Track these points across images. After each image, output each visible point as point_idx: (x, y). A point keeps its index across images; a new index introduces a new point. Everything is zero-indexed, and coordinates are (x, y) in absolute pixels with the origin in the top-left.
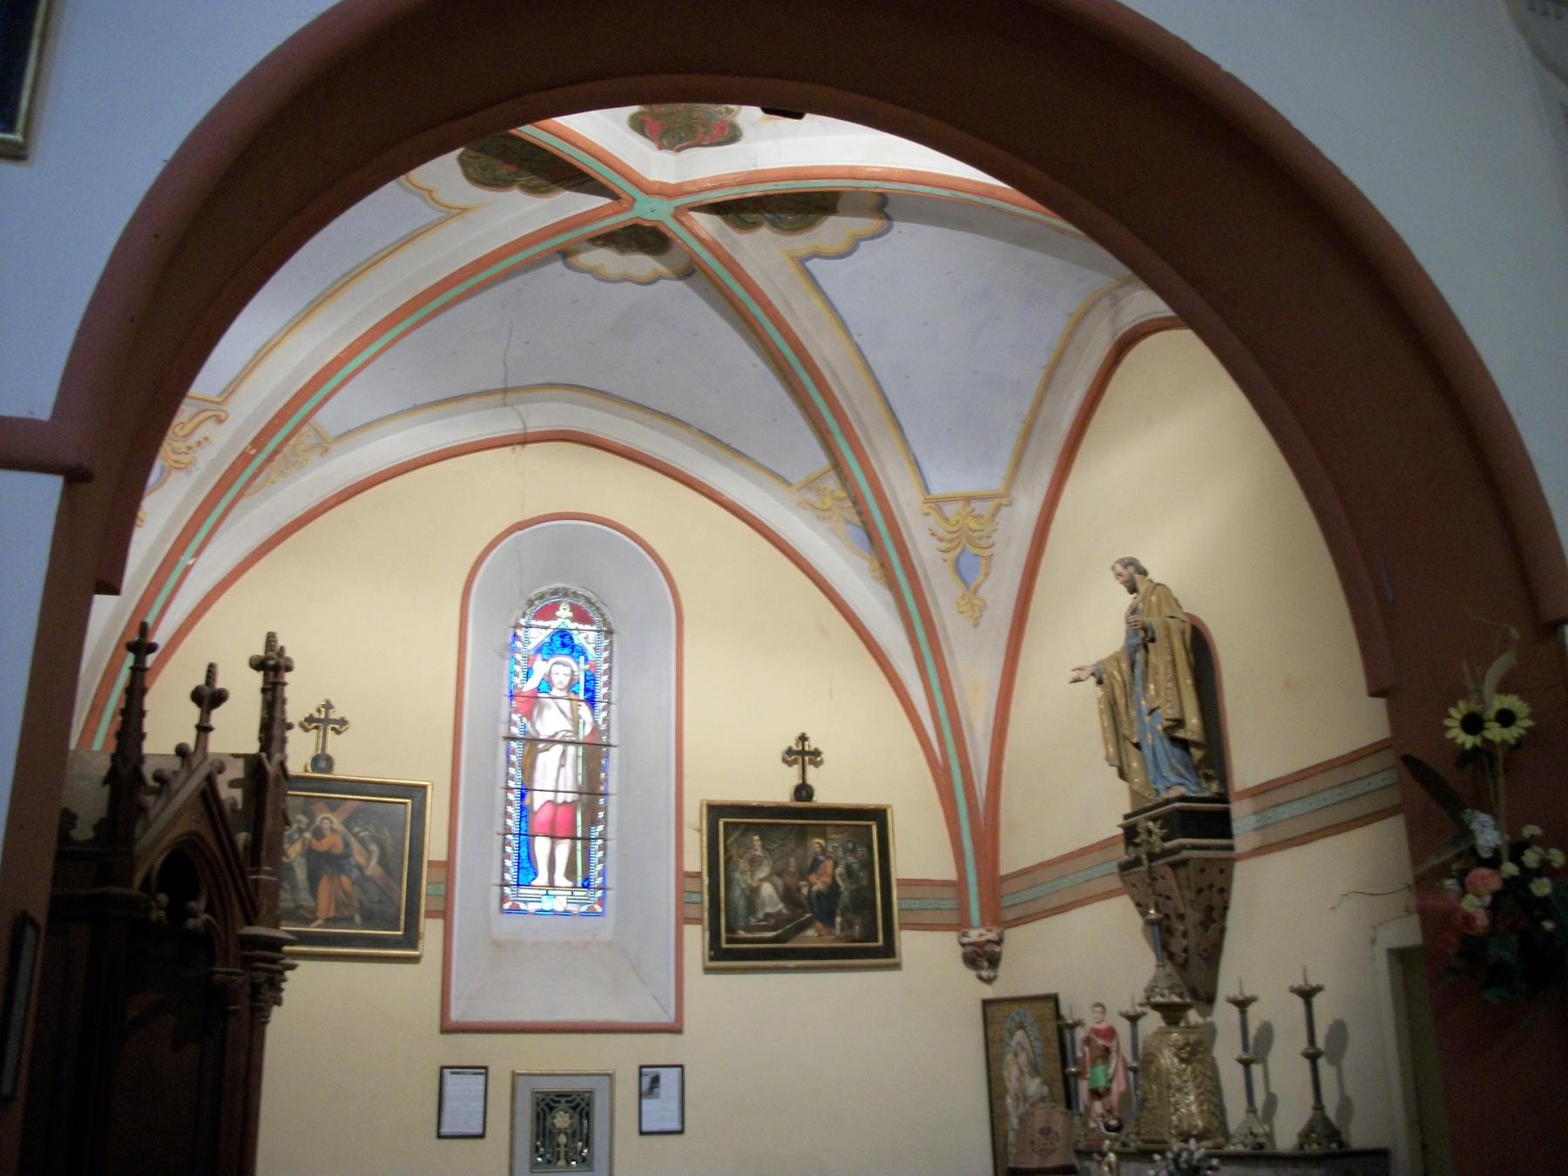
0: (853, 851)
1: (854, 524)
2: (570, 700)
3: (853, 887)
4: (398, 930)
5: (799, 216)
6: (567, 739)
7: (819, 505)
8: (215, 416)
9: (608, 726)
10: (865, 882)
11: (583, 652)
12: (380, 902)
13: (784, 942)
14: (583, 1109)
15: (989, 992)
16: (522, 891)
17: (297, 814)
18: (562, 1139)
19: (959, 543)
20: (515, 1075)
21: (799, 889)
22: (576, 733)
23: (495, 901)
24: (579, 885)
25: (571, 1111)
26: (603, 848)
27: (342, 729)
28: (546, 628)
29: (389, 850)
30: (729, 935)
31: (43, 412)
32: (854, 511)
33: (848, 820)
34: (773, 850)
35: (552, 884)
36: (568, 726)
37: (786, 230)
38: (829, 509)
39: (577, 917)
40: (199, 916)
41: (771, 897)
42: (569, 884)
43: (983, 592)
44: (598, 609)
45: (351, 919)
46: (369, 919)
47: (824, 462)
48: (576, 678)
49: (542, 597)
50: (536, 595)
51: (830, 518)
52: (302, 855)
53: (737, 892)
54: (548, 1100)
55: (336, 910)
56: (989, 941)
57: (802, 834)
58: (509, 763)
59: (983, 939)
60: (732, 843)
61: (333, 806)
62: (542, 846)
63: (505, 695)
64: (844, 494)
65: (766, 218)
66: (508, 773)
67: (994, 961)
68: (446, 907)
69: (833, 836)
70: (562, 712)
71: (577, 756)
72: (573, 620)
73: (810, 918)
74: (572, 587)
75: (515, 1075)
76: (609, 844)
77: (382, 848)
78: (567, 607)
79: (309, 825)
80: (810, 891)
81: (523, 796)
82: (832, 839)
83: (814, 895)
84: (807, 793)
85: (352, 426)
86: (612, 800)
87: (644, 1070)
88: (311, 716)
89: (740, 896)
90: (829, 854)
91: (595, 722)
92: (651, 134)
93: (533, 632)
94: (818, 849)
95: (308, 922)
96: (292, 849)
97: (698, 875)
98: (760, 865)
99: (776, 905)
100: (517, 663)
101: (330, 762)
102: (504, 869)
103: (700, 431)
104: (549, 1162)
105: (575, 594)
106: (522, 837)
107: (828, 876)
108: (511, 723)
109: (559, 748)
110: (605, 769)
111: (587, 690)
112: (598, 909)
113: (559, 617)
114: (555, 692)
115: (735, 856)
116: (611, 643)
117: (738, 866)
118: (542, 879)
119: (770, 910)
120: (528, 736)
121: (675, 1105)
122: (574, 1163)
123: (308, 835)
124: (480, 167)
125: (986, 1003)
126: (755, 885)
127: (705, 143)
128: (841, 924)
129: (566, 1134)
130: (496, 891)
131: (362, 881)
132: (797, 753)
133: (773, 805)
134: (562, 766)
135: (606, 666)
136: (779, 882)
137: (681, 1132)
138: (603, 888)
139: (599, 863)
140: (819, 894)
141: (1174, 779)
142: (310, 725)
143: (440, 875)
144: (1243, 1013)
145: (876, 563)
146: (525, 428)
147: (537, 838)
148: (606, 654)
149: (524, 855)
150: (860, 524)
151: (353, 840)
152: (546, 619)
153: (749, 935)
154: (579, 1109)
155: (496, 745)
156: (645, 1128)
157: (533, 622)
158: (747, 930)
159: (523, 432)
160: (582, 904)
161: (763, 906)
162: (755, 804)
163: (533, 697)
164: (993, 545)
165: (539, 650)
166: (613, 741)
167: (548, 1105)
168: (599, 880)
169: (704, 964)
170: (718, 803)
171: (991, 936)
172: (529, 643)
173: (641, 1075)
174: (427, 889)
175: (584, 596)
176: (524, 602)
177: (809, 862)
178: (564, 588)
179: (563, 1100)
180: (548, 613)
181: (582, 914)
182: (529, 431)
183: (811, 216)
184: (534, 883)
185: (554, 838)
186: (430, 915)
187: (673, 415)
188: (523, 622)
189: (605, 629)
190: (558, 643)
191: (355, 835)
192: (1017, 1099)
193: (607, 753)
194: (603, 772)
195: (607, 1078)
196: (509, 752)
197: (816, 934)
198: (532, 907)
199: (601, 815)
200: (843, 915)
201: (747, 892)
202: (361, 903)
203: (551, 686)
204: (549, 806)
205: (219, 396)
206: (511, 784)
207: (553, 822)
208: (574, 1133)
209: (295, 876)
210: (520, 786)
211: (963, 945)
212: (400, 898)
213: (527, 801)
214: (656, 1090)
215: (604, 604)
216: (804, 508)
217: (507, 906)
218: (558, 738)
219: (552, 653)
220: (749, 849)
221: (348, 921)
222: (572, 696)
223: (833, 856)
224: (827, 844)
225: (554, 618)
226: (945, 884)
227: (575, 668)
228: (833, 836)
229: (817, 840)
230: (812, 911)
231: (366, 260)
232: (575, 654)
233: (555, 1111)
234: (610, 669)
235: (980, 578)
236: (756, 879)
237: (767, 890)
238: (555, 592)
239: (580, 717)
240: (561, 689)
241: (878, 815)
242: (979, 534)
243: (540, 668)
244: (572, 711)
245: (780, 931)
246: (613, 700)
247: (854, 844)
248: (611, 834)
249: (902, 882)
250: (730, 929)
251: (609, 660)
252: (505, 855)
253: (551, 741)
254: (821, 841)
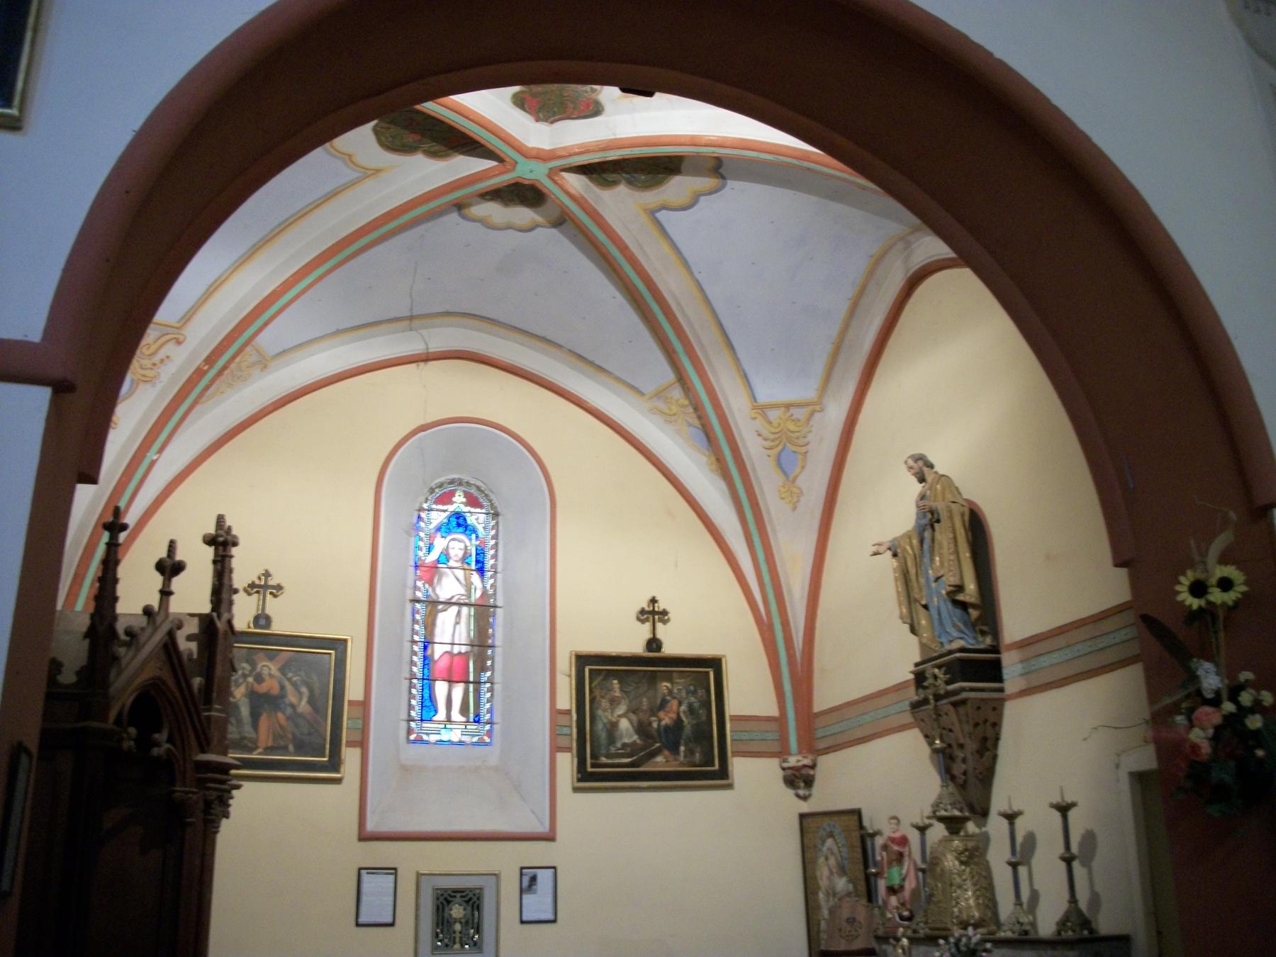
0: (694, 693)
1: (695, 427)
2: (464, 569)
3: (694, 722)
4: (324, 757)
5: (650, 175)
6: (462, 601)
7: (667, 411)
8: (175, 338)
9: (495, 591)
10: (704, 718)
11: (474, 531)
12: (309, 734)
13: (638, 767)
14: (475, 902)
15: (805, 807)
16: (424, 725)
17: (242, 662)
18: (458, 927)
19: (781, 442)
20: (419, 875)
21: (650, 724)
22: (469, 596)
23: (403, 733)
24: (472, 720)
25: (465, 904)
26: (491, 690)
27: (279, 594)
28: (444, 511)
29: (317, 692)
30: (593, 761)
31: (35, 335)
32: (695, 416)
33: (690, 667)
34: (629, 692)
35: (449, 720)
36: (462, 591)
37: (640, 187)
38: (674, 415)
39: (470, 746)
40: (162, 745)
41: (627, 730)
42: (463, 719)
43: (800, 482)
44: (486, 495)
45: (286, 748)
46: (301, 748)
47: (671, 376)
48: (468, 551)
49: (441, 486)
50: (436, 484)
51: (676, 421)
52: (246, 696)
53: (600, 726)
54: (446, 895)
55: (274, 740)
56: (805, 766)
57: (653, 679)
58: (415, 621)
59: (800, 764)
60: (596, 686)
61: (271, 656)
62: (441, 688)
63: (411, 566)
64: (686, 402)
65: (624, 177)
66: (413, 629)
67: (809, 782)
68: (363, 738)
69: (678, 681)
70: (458, 580)
71: (470, 615)
72: (467, 504)
73: (659, 747)
74: (466, 478)
75: (419, 875)
76: (496, 687)
77: (311, 690)
78: (462, 494)
79: (251, 671)
80: (659, 725)
81: (425, 648)
82: (677, 683)
83: (662, 728)
84: (657, 645)
85: (286, 347)
86: (498, 651)
87: (524, 871)
88: (253, 582)
89: (602, 730)
90: (674, 695)
91: (484, 587)
92: (530, 109)
93: (434, 514)
94: (666, 691)
95: (251, 750)
96: (237, 691)
97: (568, 712)
98: (619, 704)
99: (632, 736)
100: (421, 539)
101: (268, 620)
102: (411, 707)
103: (570, 351)
104: (447, 945)
105: (468, 484)
106: (425, 681)
107: (674, 713)
108: (416, 588)
109: (455, 609)
110: (492, 626)
111: (477, 562)
112: (487, 739)
113: (455, 502)
114: (452, 563)
115: (598, 697)
116: (497, 523)
117: (600, 705)
118: (441, 715)
119: (626, 740)
120: (430, 599)
121: (549, 900)
122: (467, 946)
123: (250, 679)
124: (391, 136)
125: (803, 817)
126: (614, 720)
127: (574, 116)
128: (685, 752)
129: (461, 923)
130: (404, 725)
131: (295, 717)
132: (649, 612)
133: (629, 655)
134: (457, 623)
135: (493, 542)
136: (634, 717)
137: (554, 921)
138: (490, 722)
139: (487, 703)
140: (667, 728)
141: (955, 634)
142: (252, 590)
143: (358, 712)
144: (1012, 824)
145: (713, 458)
146: (427, 349)
147: (437, 682)
148: (493, 532)
149: (426, 695)
150: (700, 426)
151: (287, 684)
152: (444, 504)
153: (610, 761)
154: (471, 902)
155: (404, 606)
156: (525, 918)
157: (434, 506)
158: (608, 757)
159: (426, 351)
160: (473, 736)
161: (621, 737)
162: (614, 654)
163: (434, 568)
164: (808, 444)
165: (438, 529)
166: (499, 603)
167: (446, 899)
168: (488, 717)
169: (573, 784)
170: (584, 653)
171: (807, 761)
172: (431, 523)
173: (521, 874)
174: (347, 724)
175: (475, 485)
176: (427, 490)
177: (659, 701)
178: (459, 479)
179: (458, 895)
180: (446, 499)
181: (473, 744)
182: (430, 351)
183: (660, 176)
184: (434, 718)
185: (451, 682)
186: (350, 744)
187: (548, 338)
188: (425, 506)
189: (492, 512)
190: (454, 523)
191: (289, 680)
192: (828, 894)
193: (494, 612)
194: (491, 628)
195: (494, 877)
196: (414, 612)
197: (664, 760)
198: (433, 738)
199: (489, 663)
200: (686, 745)
201: (608, 726)
202: (294, 735)
203: (448, 559)
204: (447, 656)
205: (178, 322)
206: (416, 638)
207: (450, 669)
208: (467, 922)
209: (240, 713)
210: (423, 640)
211: (784, 769)
212: (326, 731)
213: (429, 652)
214: (534, 887)
215: (491, 491)
216: (655, 414)
217: (413, 737)
218: (454, 600)
219: (449, 532)
220: (610, 691)
221: (283, 750)
222: (466, 566)
223: (678, 696)
224: (673, 687)
225: (451, 503)
226: (769, 719)
227: (468, 544)
228: (678, 681)
229: (665, 684)
230: (661, 741)
231: (298, 212)
232: (468, 532)
233: (452, 904)
234: (496, 544)
235: (798, 470)
236: (615, 715)
237: (624, 724)
238: (452, 482)
239: (472, 583)
240: (456, 561)
241: (715, 664)
242: (797, 434)
243: (440, 543)
244: (466, 579)
245: (635, 758)
246: (499, 569)
247: (695, 687)
248: (498, 678)
249: (734, 718)
250: (594, 756)
251: (495, 537)
252: (411, 696)
253: (449, 603)
254: (668, 685)
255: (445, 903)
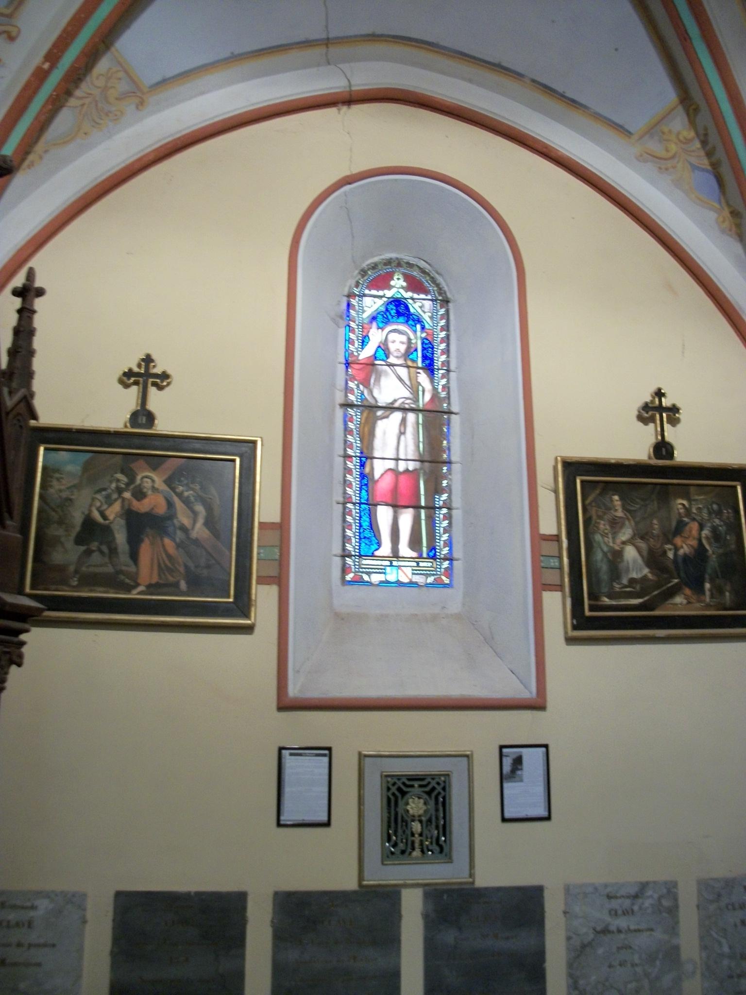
0: (719, 513)
1: (703, 170)
2: (408, 367)
3: (721, 551)
4: (229, 597)
6: (407, 406)
7: (663, 154)
8: (5, 32)
9: (448, 393)
10: (733, 547)
11: (419, 321)
12: (208, 567)
13: (652, 609)
14: (439, 793)
16: (364, 562)
17: (116, 473)
18: (417, 827)
20: (362, 757)
21: (665, 553)
22: (416, 400)
23: (336, 572)
24: (425, 555)
25: (425, 796)
26: (449, 517)
27: (165, 384)
28: (380, 297)
29: (217, 511)
30: (593, 602)
32: (702, 153)
33: (713, 480)
34: (635, 511)
35: (395, 554)
36: (407, 394)
38: (673, 157)
39: (425, 589)
41: (635, 561)
42: (414, 554)
44: (433, 280)
45: (176, 585)
47: (671, 95)
48: (413, 345)
49: (374, 267)
50: (367, 266)
51: (674, 167)
52: (121, 516)
53: (599, 556)
54: (399, 784)
55: (159, 575)
57: (664, 495)
58: (347, 431)
60: (590, 504)
61: (155, 462)
62: (384, 514)
63: (340, 363)
64: (692, 134)
66: (345, 441)
68: (280, 574)
69: (697, 497)
70: (400, 379)
71: (418, 423)
72: (407, 289)
73: (677, 584)
74: (406, 257)
75: (362, 757)
76: (455, 513)
77: (209, 509)
78: (401, 277)
79: (128, 485)
80: (675, 555)
81: (362, 465)
82: (695, 500)
83: (680, 560)
84: (667, 451)
85: (169, 74)
86: (456, 468)
87: (505, 750)
88: (130, 370)
89: (602, 561)
90: (693, 515)
91: (435, 389)
93: (367, 301)
94: (682, 511)
95: (128, 589)
96: (110, 509)
97: (557, 538)
98: (621, 527)
99: (641, 570)
100: (352, 330)
101: (150, 418)
102: (345, 539)
103: (533, 81)
104: (403, 852)
105: (410, 265)
106: (363, 506)
107: (694, 538)
108: (347, 390)
109: (397, 416)
110: (447, 437)
111: (425, 357)
112: (446, 580)
113: (394, 287)
114: (392, 360)
115: (594, 517)
116: (447, 311)
117: (597, 528)
118: (386, 549)
119: (634, 575)
120: (366, 403)
121: (540, 789)
122: (430, 853)
123: (127, 495)
126: (617, 548)
128: (711, 590)
129: (421, 821)
130: (338, 561)
131: (188, 544)
133: (631, 463)
134: (402, 433)
135: (443, 334)
136: (643, 545)
137: (548, 818)
138: (450, 558)
139: (444, 533)
140: (686, 558)
142: (129, 379)
143: (273, 537)
145: (726, 212)
146: (350, 86)
147: (379, 507)
148: (443, 323)
149: (366, 524)
150: (709, 168)
151: (176, 500)
152: (378, 288)
153: (614, 603)
154: (434, 795)
155: (333, 411)
156: (507, 815)
157: (367, 292)
158: (610, 597)
159: (348, 89)
160: (427, 576)
161: (628, 570)
162: (613, 461)
163: (370, 364)
165: (374, 318)
166: (455, 408)
167: (399, 789)
168: (445, 551)
169: (566, 633)
170: (574, 460)
172: (364, 311)
173: (501, 755)
174: (258, 554)
175: (417, 266)
176: (357, 272)
178: (397, 259)
179: (416, 784)
180: (382, 282)
181: (427, 585)
182: (353, 88)
184: (377, 553)
185: (396, 507)
186: (261, 580)
187: (504, 64)
188: (356, 291)
189: (440, 298)
190: (393, 312)
191: (180, 495)
193: (449, 420)
194: (445, 439)
195: (465, 759)
196: (346, 419)
197: (685, 602)
198: (376, 578)
199: (445, 483)
200: (712, 581)
201: (610, 556)
202: (186, 567)
203: (387, 354)
204: (390, 474)
205: (7, 7)
206: (350, 452)
207: (395, 490)
208: (429, 821)
209: (114, 539)
210: (358, 455)
213: (367, 470)
214: (519, 772)
215: (438, 273)
216: (645, 161)
217: (349, 577)
218: (397, 405)
219: (387, 322)
220: (610, 509)
221: (174, 587)
222: (410, 363)
223: (698, 518)
224: (690, 505)
225: (389, 287)
227: (412, 336)
228: (697, 497)
229: (680, 501)
230: (679, 577)
232: (411, 322)
233: (408, 796)
234: (448, 337)
236: (618, 541)
237: (630, 553)
238: (388, 262)
239: (419, 384)
240: (397, 357)
243: (376, 336)
244: (410, 379)
245: (646, 598)
246: (453, 366)
248: (456, 502)
250: (593, 596)
251: (447, 328)
252: (345, 525)
253: (390, 408)
254: (685, 502)
255: (428, 789)
